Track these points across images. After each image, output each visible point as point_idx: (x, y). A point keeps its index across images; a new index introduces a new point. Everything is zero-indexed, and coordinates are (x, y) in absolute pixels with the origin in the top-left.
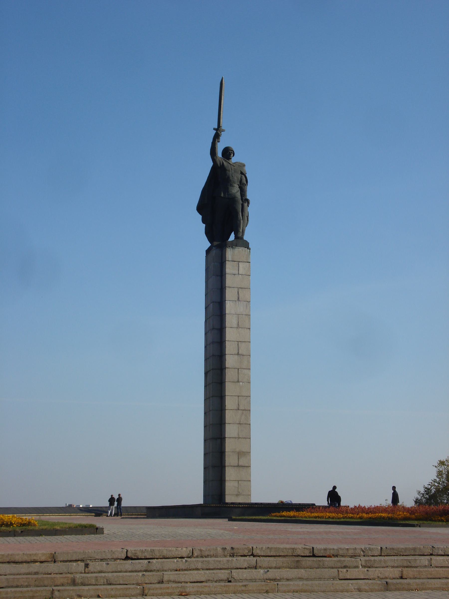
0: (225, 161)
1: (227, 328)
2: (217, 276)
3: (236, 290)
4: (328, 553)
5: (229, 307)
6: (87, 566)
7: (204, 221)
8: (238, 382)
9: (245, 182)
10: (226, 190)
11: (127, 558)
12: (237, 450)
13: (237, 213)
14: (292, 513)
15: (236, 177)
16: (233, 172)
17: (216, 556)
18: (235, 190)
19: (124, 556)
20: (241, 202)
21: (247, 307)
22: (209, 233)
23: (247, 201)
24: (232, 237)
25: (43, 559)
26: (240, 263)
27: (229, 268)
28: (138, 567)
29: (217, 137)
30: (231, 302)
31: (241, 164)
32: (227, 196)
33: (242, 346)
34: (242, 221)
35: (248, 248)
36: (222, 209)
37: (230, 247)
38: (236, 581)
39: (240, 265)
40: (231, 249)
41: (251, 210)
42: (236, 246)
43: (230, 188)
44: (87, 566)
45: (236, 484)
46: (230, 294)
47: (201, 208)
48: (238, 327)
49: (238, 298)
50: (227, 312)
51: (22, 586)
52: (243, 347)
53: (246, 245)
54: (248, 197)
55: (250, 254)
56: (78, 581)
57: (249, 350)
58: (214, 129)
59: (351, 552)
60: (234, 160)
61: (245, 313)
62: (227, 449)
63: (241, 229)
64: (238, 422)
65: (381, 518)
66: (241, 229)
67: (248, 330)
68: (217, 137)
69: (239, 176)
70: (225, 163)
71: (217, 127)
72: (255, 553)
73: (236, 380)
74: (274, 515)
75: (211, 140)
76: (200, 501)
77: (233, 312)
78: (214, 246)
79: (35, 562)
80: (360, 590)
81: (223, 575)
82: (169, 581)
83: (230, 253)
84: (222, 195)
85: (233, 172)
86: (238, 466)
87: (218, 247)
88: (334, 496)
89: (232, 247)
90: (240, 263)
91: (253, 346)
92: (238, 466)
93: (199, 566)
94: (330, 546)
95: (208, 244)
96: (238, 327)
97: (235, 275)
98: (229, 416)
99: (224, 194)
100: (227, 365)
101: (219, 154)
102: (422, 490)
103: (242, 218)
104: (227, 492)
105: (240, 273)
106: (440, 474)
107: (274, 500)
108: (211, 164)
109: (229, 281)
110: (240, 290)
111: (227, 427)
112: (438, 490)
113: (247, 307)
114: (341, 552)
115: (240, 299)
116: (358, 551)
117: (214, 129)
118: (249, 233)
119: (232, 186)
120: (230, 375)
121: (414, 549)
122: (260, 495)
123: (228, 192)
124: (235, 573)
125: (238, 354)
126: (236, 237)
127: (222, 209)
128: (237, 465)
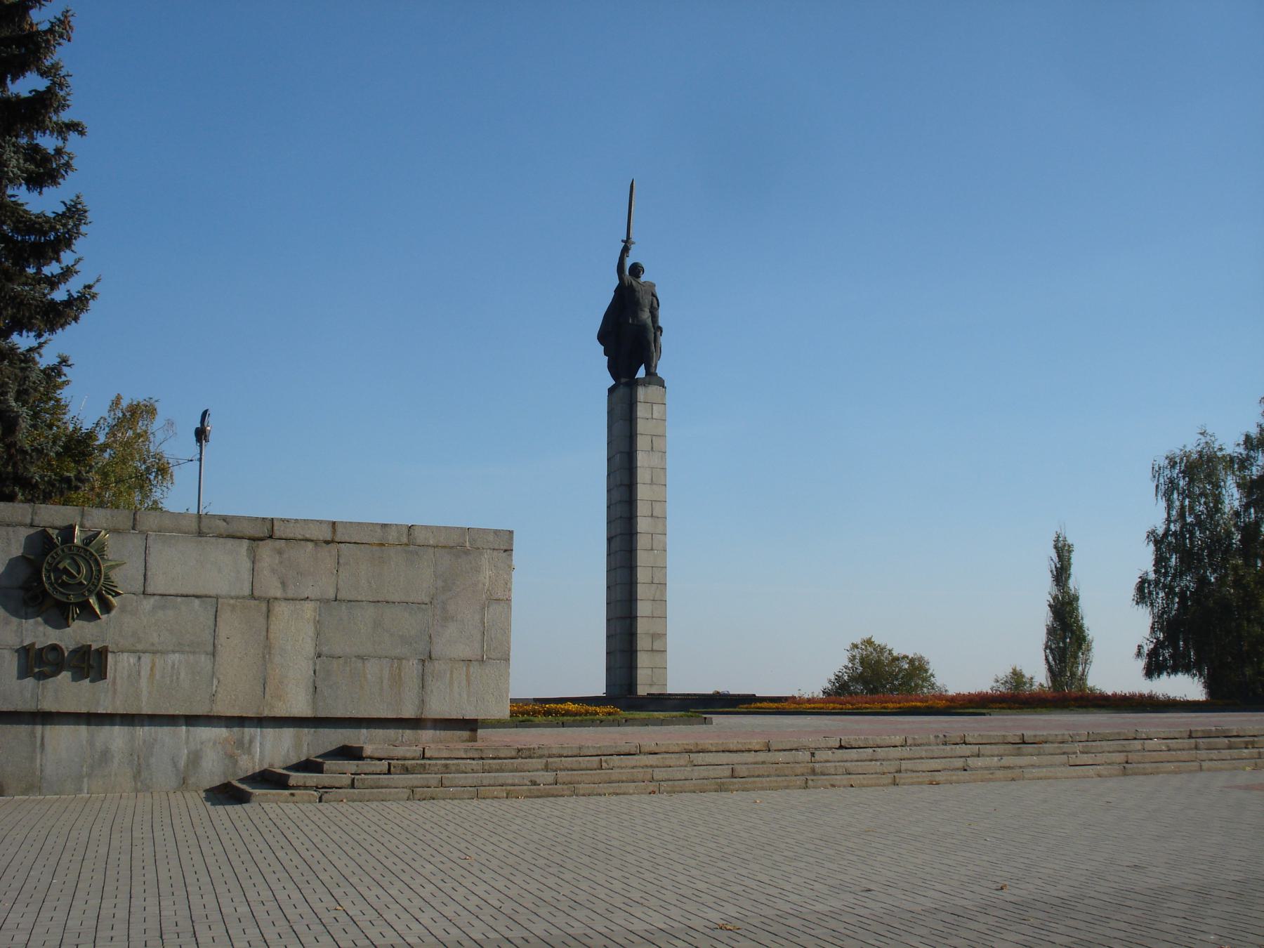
4: (1037, 740)
5: (642, 459)
6: (813, 755)
10: (635, 315)
11: (841, 747)
13: (649, 343)
14: (780, 705)
15: (646, 300)
17: (929, 745)
18: (646, 315)
19: (837, 745)
22: (613, 368)
23: (660, 329)
24: (641, 373)
25: (757, 748)
27: (641, 411)
28: (864, 756)
29: (625, 250)
36: (629, 337)
38: (972, 769)
41: (664, 340)
44: (813, 755)
45: (649, 671)
46: (642, 443)
48: (652, 483)
51: (762, 776)
52: (657, 506)
53: (661, 383)
56: (818, 770)
59: (1059, 739)
60: (643, 278)
65: (916, 707)
68: (625, 250)
72: (968, 739)
74: (743, 708)
79: (750, 751)
80: (1099, 776)
81: (959, 763)
82: (906, 771)
83: (641, 393)
87: (627, 384)
93: (924, 754)
94: (1039, 733)
96: (652, 483)
98: (641, 591)
102: (833, 678)
106: (852, 659)
107: (708, 690)
108: (615, 282)
109: (641, 426)
112: (852, 679)
114: (1050, 739)
116: (1067, 737)
118: (663, 368)
120: (642, 542)
121: (1119, 734)
122: (679, 682)
124: (970, 761)
126: (648, 372)
127: (629, 337)
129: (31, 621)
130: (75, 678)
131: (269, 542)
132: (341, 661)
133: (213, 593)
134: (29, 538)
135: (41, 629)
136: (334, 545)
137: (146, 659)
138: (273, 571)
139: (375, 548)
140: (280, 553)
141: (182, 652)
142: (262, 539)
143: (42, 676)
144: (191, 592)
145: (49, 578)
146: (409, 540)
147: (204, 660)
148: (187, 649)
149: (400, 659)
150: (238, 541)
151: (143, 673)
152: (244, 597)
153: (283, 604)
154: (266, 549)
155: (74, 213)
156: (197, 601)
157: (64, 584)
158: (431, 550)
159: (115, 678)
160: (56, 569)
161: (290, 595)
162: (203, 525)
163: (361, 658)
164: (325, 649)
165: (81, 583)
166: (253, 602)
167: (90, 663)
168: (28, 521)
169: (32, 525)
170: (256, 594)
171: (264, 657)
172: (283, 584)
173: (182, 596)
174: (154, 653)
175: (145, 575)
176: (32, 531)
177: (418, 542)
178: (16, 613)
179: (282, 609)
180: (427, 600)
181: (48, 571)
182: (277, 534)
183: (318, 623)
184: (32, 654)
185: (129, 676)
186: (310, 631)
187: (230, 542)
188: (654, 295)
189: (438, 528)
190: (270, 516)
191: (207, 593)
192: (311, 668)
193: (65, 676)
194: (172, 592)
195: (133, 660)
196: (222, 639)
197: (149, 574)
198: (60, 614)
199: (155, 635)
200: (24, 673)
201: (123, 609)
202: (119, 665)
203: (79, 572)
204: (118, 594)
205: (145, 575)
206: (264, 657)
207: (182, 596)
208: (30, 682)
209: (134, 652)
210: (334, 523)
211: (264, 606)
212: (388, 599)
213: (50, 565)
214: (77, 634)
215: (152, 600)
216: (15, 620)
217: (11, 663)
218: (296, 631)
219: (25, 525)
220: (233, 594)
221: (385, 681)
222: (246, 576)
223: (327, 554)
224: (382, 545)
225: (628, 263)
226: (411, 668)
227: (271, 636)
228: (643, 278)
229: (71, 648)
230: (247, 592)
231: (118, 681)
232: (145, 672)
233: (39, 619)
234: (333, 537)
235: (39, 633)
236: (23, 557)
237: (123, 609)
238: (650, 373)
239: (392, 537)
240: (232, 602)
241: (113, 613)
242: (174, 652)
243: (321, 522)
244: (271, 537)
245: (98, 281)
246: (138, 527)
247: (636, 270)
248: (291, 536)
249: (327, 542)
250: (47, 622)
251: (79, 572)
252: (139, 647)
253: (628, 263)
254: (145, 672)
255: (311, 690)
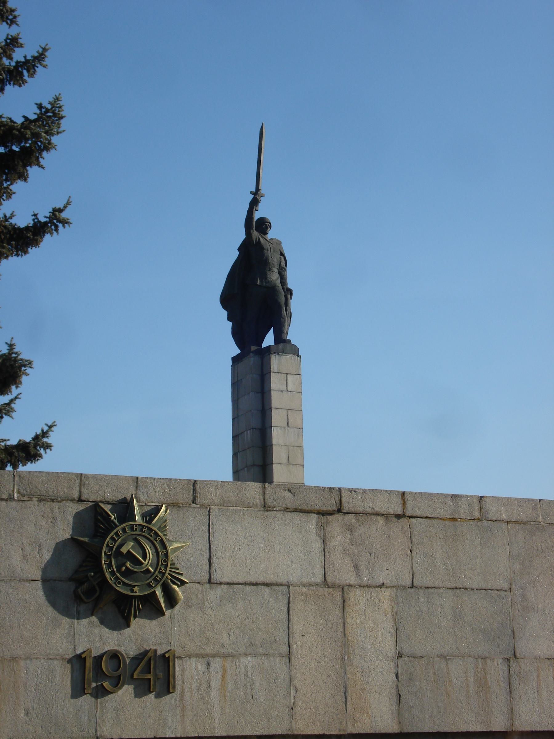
0: (262, 237)
1: (274, 465)
2: (257, 392)
3: (284, 412)
7: (229, 319)
9: (285, 266)
10: (264, 276)
15: (274, 260)
16: (272, 251)
18: (274, 277)
21: (298, 436)
22: (239, 336)
23: (290, 291)
24: (269, 340)
26: (288, 376)
27: (275, 382)
29: (254, 203)
30: (278, 429)
31: (278, 241)
32: (264, 284)
35: (298, 355)
36: (255, 299)
37: (275, 353)
39: (289, 379)
40: (277, 356)
41: (294, 304)
42: (283, 352)
43: (269, 273)
47: (226, 300)
48: (288, 463)
50: (274, 442)
53: (295, 352)
55: (300, 364)
58: (251, 193)
63: (286, 329)
67: (301, 467)
68: (254, 203)
69: (279, 256)
75: (247, 208)
76: (121, 550)
78: (252, 352)
83: (275, 362)
85: (272, 251)
89: (278, 354)
90: (288, 376)
95: (236, 351)
96: (288, 463)
97: (282, 391)
99: (261, 281)
105: (289, 389)
108: (241, 236)
109: (276, 400)
110: (290, 412)
113: (298, 436)
115: (290, 425)
117: (251, 193)
119: (271, 270)
123: (266, 279)
127: (255, 299)
129: (84, 621)
130: (140, 693)
131: (338, 516)
132: (423, 661)
133: (284, 580)
134: (78, 516)
135: (96, 631)
136: (404, 521)
137: (216, 664)
138: (346, 552)
139: (448, 523)
140: (350, 529)
141: (255, 655)
142: (330, 513)
143: (101, 692)
144: (261, 579)
145: (110, 565)
146: (475, 515)
147: (280, 665)
148: (261, 650)
149: (484, 658)
150: (305, 515)
151: (214, 684)
152: (317, 585)
153: (359, 592)
154: (336, 524)
155: (49, 117)
156: (267, 590)
157: (128, 573)
158: (504, 525)
159: (183, 692)
160: (118, 553)
161: (365, 580)
162: (267, 496)
163: (443, 657)
164: (406, 649)
165: (148, 571)
166: (327, 590)
167: (154, 673)
168: (76, 495)
169: (80, 500)
170: (330, 580)
171: (343, 659)
172: (356, 567)
173: (251, 584)
174: (224, 656)
175: (210, 559)
176: (81, 507)
177: (492, 516)
178: (66, 612)
179: (357, 598)
180: (506, 586)
181: (108, 557)
182: (346, 507)
183: (396, 617)
184: (89, 663)
185: (199, 689)
186: (389, 626)
187: (298, 517)
188: (282, 254)
189: (510, 499)
190: (337, 485)
191: (279, 580)
192: (393, 670)
193: (127, 690)
194: (240, 580)
195: (201, 667)
196: (296, 638)
197: (214, 557)
198: (121, 610)
199: (225, 635)
200: (79, 689)
201: (188, 604)
202: (187, 672)
203: (145, 558)
204: (183, 583)
205: (210, 559)
206: (343, 659)
207: (251, 584)
208: (86, 700)
209: (202, 656)
210: (403, 494)
211: (338, 595)
212: (468, 585)
213: (111, 549)
214: (140, 635)
215: (219, 590)
216: (65, 621)
217: (63, 677)
218: (373, 624)
219: (72, 500)
220: (305, 580)
221: (471, 687)
222: (318, 559)
223: (398, 529)
224: (454, 520)
225: (257, 215)
226: (497, 669)
227: (349, 632)
228: (271, 234)
229: (132, 654)
230: (319, 578)
231: (187, 695)
232: (215, 683)
233: (94, 619)
234: (404, 511)
235: (94, 636)
236: (73, 540)
237: (188, 604)
238: (280, 338)
239: (464, 511)
240: (305, 590)
241: (177, 607)
242: (246, 655)
243: (389, 492)
244: (339, 511)
245: (68, 203)
246: (199, 500)
247: (263, 225)
248: (361, 509)
249: (398, 517)
250: (102, 622)
251: (145, 558)
252: (209, 650)
253: (257, 215)
254: (215, 683)
255: (395, 699)
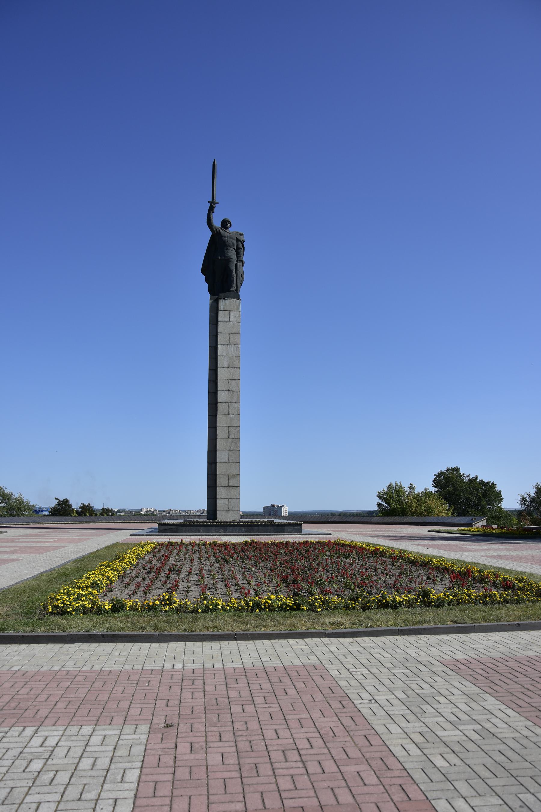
7: (207, 281)
8: (229, 414)
10: (223, 254)
12: (228, 473)
13: (231, 271)
20: (235, 262)
29: (211, 209)
33: (233, 383)
34: (235, 278)
36: (221, 272)
42: (228, 298)
45: (226, 502)
49: (229, 342)
54: (244, 259)
57: (238, 386)
58: (209, 202)
60: (230, 230)
61: (235, 355)
62: (218, 472)
64: (228, 449)
66: (235, 285)
68: (211, 209)
70: (221, 230)
71: (211, 200)
73: (227, 413)
77: (224, 354)
83: (222, 304)
84: (219, 258)
86: (228, 486)
88: (435, 475)
89: (224, 299)
91: (242, 383)
92: (228, 486)
96: (229, 366)
100: (218, 400)
101: (217, 223)
103: (235, 275)
104: (218, 508)
110: (231, 335)
111: (219, 453)
117: (209, 202)
125: (229, 390)
127: (221, 272)
128: (227, 485)
